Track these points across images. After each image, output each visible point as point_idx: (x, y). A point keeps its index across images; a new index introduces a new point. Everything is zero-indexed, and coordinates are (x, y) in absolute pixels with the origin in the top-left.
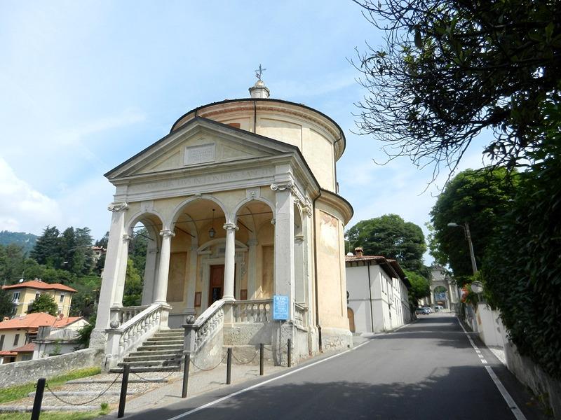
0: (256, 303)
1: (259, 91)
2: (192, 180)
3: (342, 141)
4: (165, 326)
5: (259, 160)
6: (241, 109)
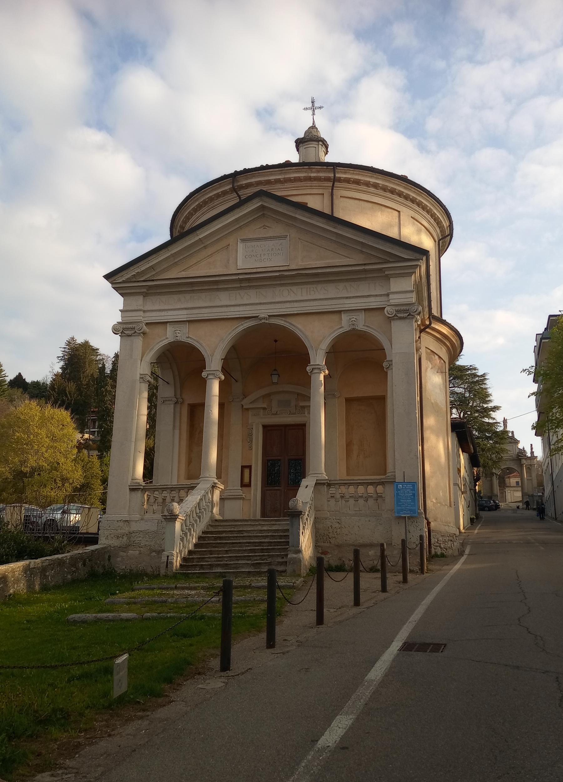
1: (314, 144)
2: (252, 292)
5: (367, 267)
6: (310, 179)
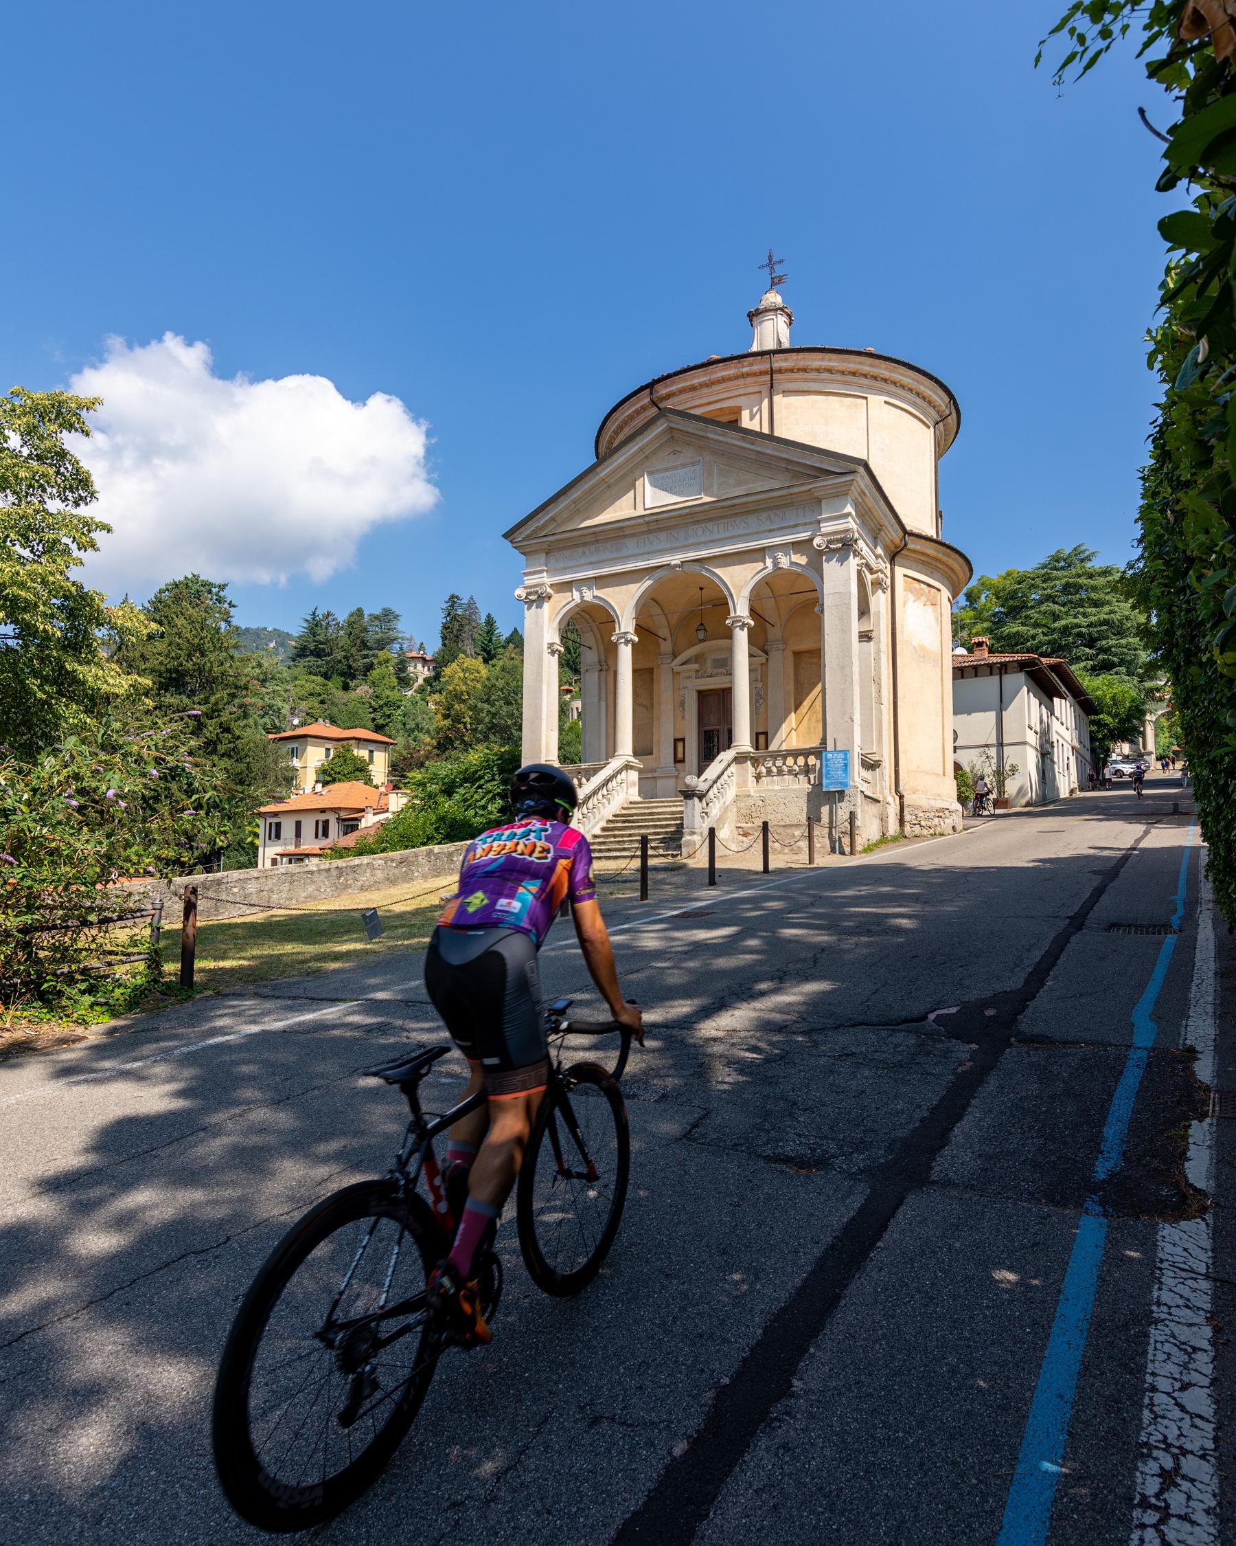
0: (801, 754)
3: (952, 419)
4: (634, 794)
6: (743, 376)
